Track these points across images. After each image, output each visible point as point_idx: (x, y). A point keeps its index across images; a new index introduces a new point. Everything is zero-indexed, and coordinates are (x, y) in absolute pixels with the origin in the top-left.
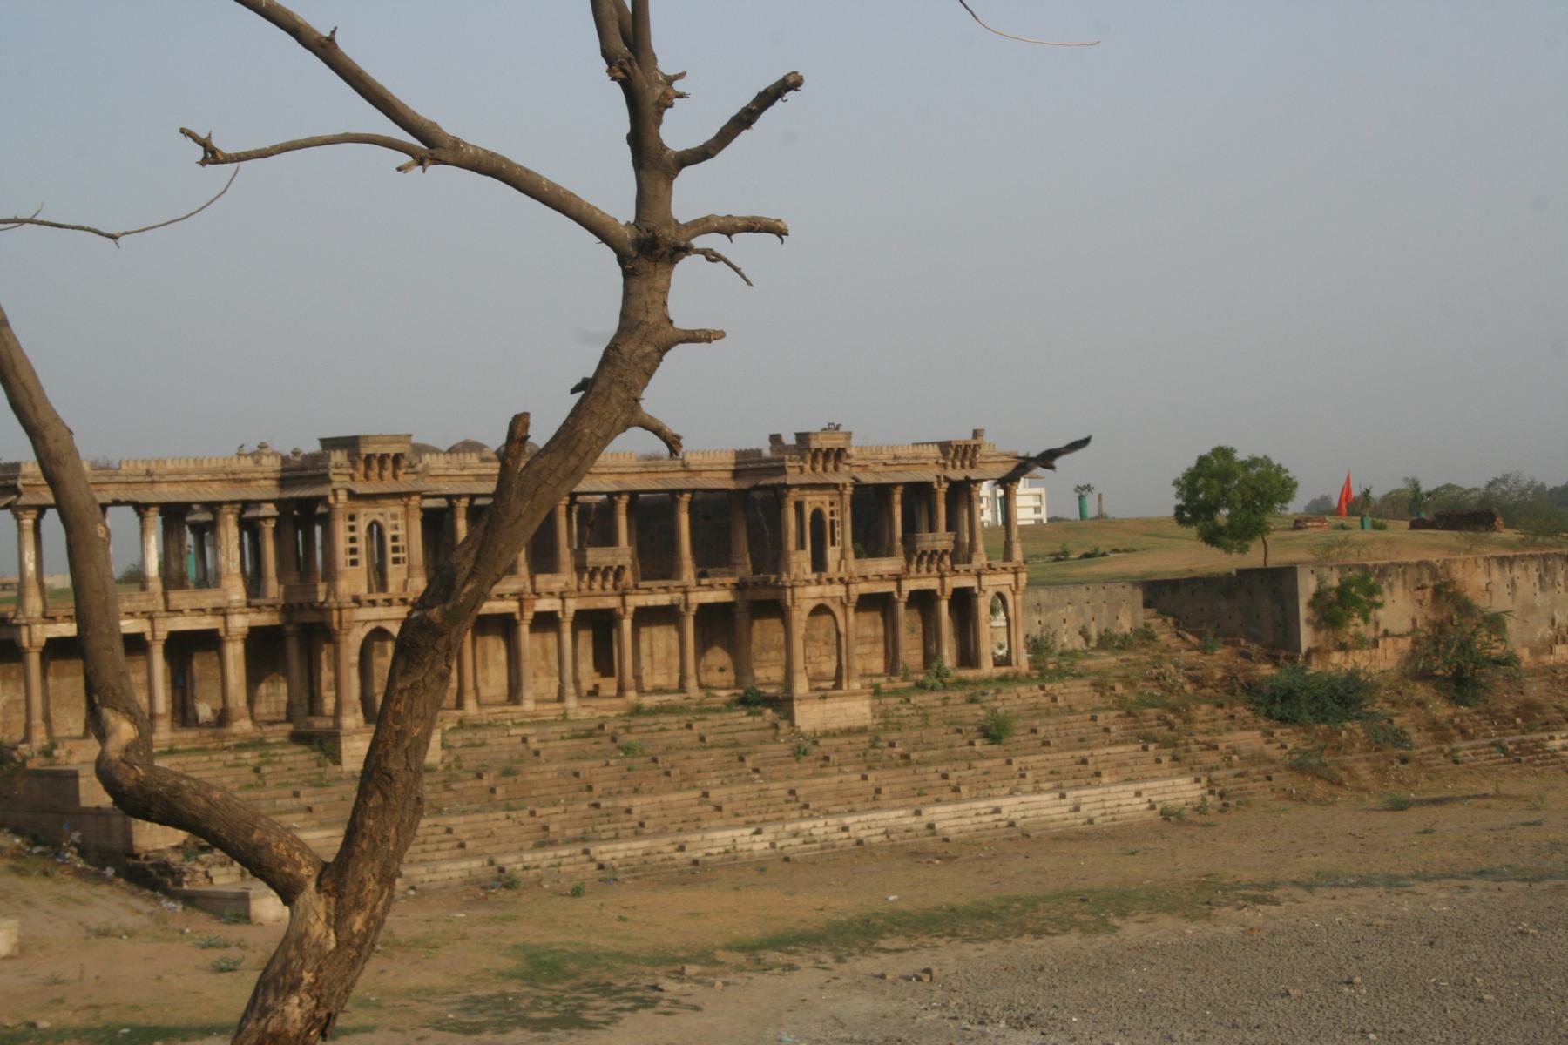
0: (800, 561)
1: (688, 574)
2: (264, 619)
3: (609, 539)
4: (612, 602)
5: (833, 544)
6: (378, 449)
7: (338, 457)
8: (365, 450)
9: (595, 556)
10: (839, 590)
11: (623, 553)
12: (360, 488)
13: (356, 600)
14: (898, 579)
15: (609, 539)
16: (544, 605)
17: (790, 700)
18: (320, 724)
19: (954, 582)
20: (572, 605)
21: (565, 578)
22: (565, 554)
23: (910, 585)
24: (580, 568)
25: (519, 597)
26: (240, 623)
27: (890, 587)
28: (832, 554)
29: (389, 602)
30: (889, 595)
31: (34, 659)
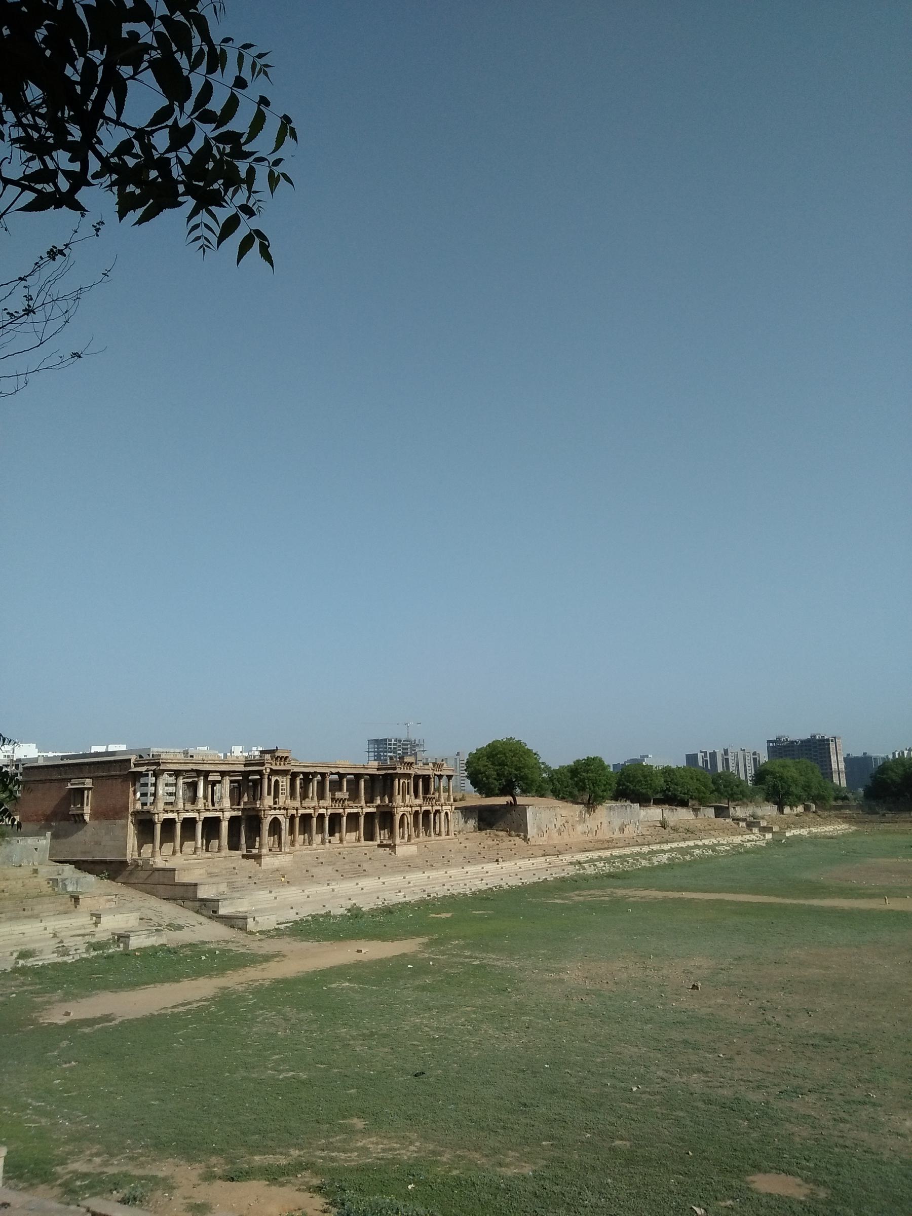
0: (399, 798)
1: (363, 803)
2: (235, 813)
3: (341, 790)
4: (341, 811)
5: (84, 784)
6: (280, 755)
7: (268, 756)
8: (277, 754)
9: (338, 795)
10: (409, 809)
11: (344, 794)
12: (274, 768)
13: (270, 807)
14: (420, 806)
15: (341, 790)
16: (322, 811)
17: (395, 845)
18: (255, 851)
19: (436, 808)
20: (330, 811)
21: (327, 802)
22: (328, 794)
23: (424, 808)
24: (333, 799)
25: (314, 808)
26: (228, 815)
27: (311, 811)
28: (407, 797)
29: (280, 809)
30: (174, 819)
31: (158, 827)
